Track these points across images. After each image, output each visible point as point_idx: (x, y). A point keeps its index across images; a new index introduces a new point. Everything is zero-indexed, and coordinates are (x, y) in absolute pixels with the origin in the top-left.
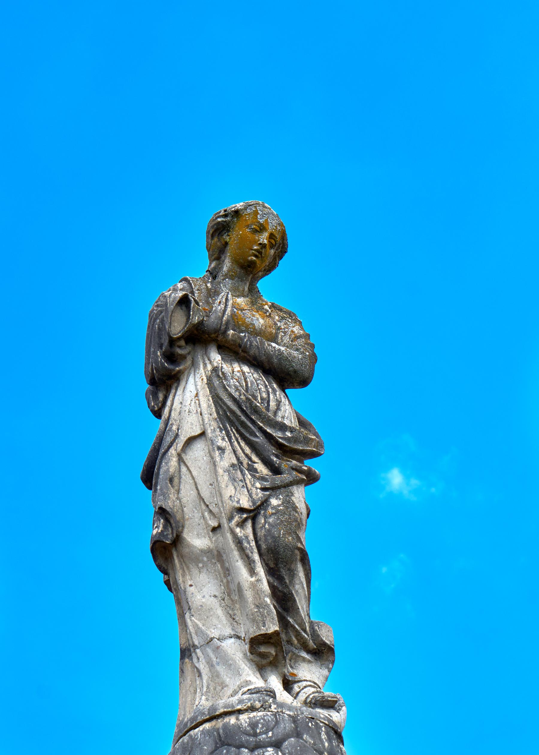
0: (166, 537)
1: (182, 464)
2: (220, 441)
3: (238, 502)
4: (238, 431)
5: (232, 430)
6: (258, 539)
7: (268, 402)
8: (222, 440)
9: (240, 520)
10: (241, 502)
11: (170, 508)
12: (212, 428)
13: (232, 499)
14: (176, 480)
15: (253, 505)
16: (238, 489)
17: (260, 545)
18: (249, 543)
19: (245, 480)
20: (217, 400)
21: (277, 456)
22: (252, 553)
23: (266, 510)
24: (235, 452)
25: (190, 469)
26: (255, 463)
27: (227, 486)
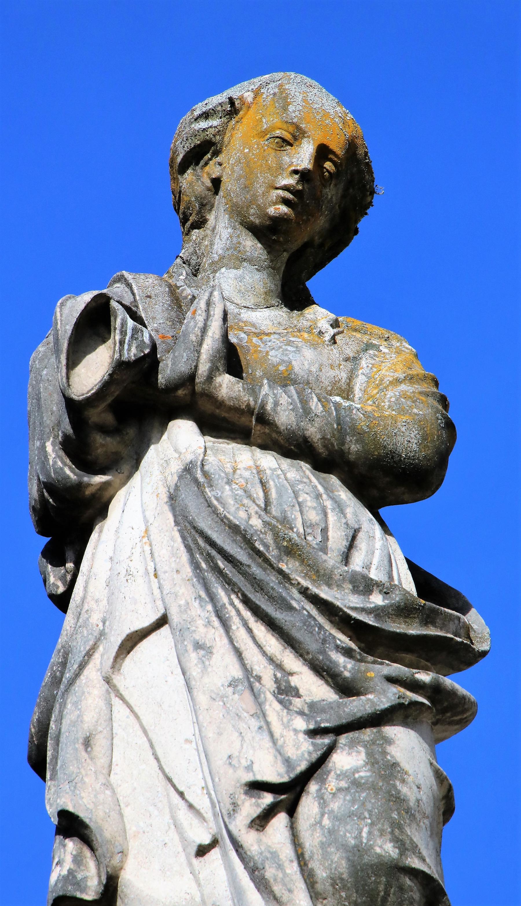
0: (80, 885)
1: (116, 702)
2: (202, 630)
3: (249, 768)
4: (246, 601)
5: (232, 604)
6: (307, 856)
7: (325, 531)
9: (256, 812)
10: (256, 767)
11: (87, 809)
12: (182, 602)
13: (234, 762)
14: (100, 744)
15: (288, 772)
16: (248, 736)
17: (312, 870)
18: (280, 867)
19: (264, 715)
20: (192, 535)
21: (348, 653)
22: (290, 891)
23: (323, 781)
24: (239, 654)
25: (136, 709)
26: (291, 674)
27: (220, 734)
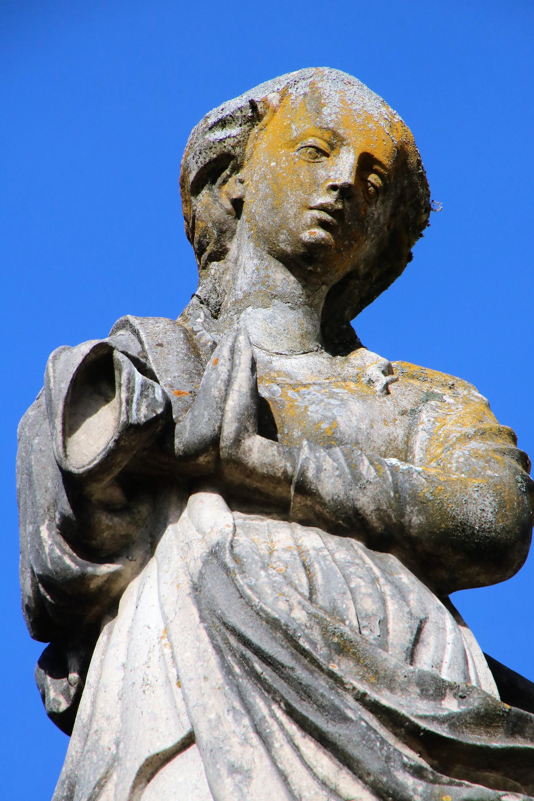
2: (238, 749)
5: (273, 716)
7: (383, 622)
8: (242, 745)
12: (213, 716)
